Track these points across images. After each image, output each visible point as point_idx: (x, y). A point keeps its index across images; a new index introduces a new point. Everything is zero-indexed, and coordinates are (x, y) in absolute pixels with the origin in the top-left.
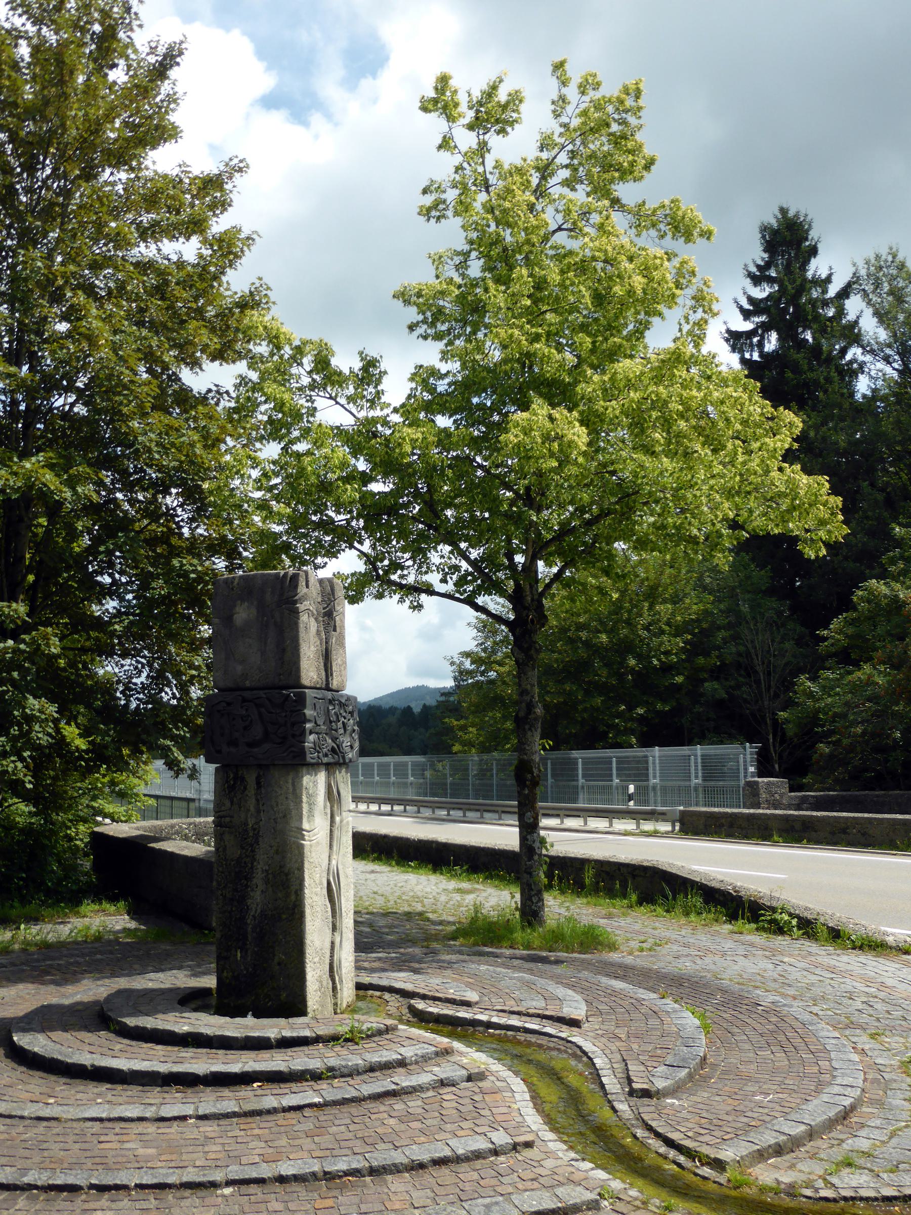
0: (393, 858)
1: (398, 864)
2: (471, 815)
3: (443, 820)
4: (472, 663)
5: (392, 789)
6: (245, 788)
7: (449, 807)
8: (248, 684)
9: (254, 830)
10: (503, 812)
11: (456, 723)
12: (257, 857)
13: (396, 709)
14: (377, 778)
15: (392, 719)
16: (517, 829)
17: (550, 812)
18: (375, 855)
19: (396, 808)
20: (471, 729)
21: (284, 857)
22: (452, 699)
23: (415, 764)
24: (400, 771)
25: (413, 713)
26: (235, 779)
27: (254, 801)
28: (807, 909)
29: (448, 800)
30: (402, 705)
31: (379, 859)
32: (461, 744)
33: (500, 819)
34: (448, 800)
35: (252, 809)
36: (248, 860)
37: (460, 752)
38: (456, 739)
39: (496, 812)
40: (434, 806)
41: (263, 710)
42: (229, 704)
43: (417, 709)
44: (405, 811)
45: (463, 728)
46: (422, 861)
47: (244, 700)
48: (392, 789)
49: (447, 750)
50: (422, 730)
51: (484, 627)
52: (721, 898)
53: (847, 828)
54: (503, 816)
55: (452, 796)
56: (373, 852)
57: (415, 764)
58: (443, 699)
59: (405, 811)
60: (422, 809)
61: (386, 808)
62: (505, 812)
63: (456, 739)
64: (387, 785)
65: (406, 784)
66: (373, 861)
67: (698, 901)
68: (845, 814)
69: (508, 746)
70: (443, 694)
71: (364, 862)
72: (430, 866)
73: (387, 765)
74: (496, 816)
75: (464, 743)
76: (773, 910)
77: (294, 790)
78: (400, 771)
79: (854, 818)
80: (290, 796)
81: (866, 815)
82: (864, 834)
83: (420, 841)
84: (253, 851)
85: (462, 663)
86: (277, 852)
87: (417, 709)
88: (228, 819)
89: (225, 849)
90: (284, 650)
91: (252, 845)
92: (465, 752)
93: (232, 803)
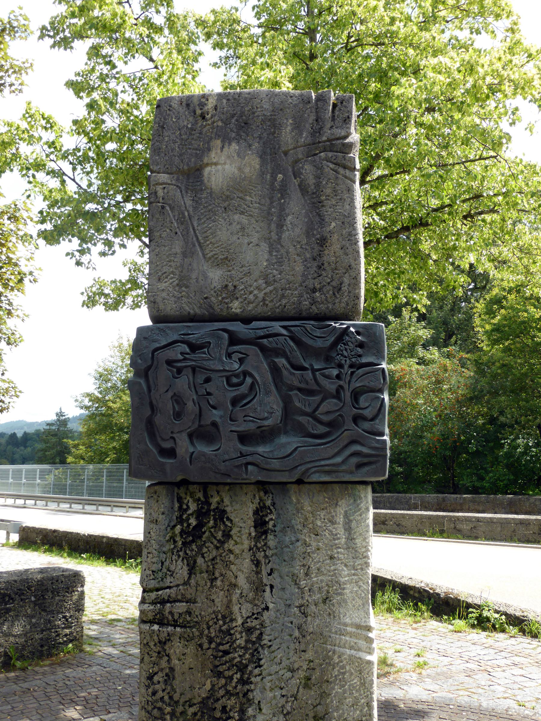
0: (64, 550)
1: (70, 555)
2: (88, 508)
3: (68, 512)
4: (90, 400)
5: (23, 488)
6: (227, 536)
7: (71, 502)
8: (236, 307)
9: (249, 631)
10: (100, 505)
11: (72, 442)
12: (256, 695)
13: (5, 434)
14: (11, 480)
15: (3, 441)
16: (142, 522)
17: (137, 506)
18: (47, 547)
19: (28, 502)
20: (81, 447)
21: (324, 695)
22: (54, 428)
23: (42, 471)
24: (31, 475)
25: (17, 437)
26: (200, 514)
27: (247, 564)
28: (471, 596)
29: (67, 496)
30: (10, 432)
31: (50, 550)
32: (74, 457)
33: (112, 511)
34: (67, 496)
35: (242, 581)
36: (231, 702)
37: (72, 462)
38: (69, 453)
39: (110, 506)
40: (59, 501)
41: (281, 361)
42: (194, 348)
43: (19, 435)
44: (35, 504)
45: (76, 446)
46: (94, 553)
47: (234, 340)
48: (23, 488)
49: (63, 462)
50: (22, 448)
51: (100, 376)
52: (417, 595)
53: (386, 521)
54: (115, 509)
55: (90, 495)
56: (43, 544)
57: (42, 471)
58: (48, 427)
59: (35, 504)
60: (49, 503)
61: (20, 502)
62: (135, 507)
63: (69, 453)
64: (33, 485)
65: (8, 483)
66: (44, 552)
67: (396, 598)
68: (383, 511)
69: (108, 459)
70: (48, 424)
71: (36, 553)
72: (103, 559)
73: (20, 471)
74: (109, 509)
75: (76, 457)
76: (478, 607)
77: (350, 539)
78: (31, 475)
79: (391, 514)
80: (342, 554)
81: (399, 512)
82: (398, 525)
83: (90, 536)
84: (244, 682)
85: (82, 401)
86: (307, 683)
87: (19, 435)
88: (181, 607)
89: (170, 677)
90: (323, 242)
91: (242, 668)
92: (75, 463)
93: (192, 569)
